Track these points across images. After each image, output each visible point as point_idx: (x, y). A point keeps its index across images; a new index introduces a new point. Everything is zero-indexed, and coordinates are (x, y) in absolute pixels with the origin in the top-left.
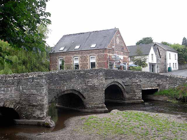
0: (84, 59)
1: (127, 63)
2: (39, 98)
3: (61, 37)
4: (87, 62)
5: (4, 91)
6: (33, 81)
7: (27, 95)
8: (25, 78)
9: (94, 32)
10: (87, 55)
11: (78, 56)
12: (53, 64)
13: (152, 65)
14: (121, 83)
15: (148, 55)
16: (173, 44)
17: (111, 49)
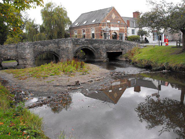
2: (25, 55)
5: (9, 51)
16: (122, 16)
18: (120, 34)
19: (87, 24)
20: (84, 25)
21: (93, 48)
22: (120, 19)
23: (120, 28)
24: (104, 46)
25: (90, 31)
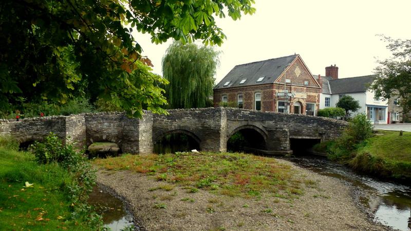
0: (249, 97)
1: (317, 103)
3: (251, 62)
18: (308, 105)
19: (247, 85)
20: (242, 85)
21: (263, 129)
22: (309, 78)
23: (309, 94)
24: (285, 126)
25: (253, 96)
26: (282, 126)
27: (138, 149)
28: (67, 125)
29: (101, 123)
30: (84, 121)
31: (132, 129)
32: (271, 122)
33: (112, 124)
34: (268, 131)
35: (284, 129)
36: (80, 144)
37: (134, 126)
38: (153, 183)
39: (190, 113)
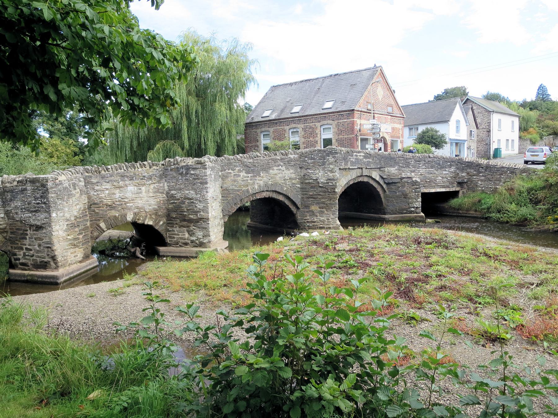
0: (311, 133)
1: (401, 139)
4: (317, 139)
6: (187, 174)
7: (178, 199)
8: (173, 167)
9: (331, 76)
10: (316, 124)
11: (299, 126)
12: (250, 145)
13: (457, 144)
14: (378, 178)
15: (446, 121)
17: (366, 111)
20: (297, 115)
26: (409, 174)
27: (207, 235)
28: (52, 196)
29: (120, 187)
30: (83, 184)
31: (190, 196)
32: (392, 169)
33: (143, 188)
34: (388, 184)
35: (414, 179)
36: (81, 236)
37: (195, 190)
38: (508, 336)
39: (282, 159)
